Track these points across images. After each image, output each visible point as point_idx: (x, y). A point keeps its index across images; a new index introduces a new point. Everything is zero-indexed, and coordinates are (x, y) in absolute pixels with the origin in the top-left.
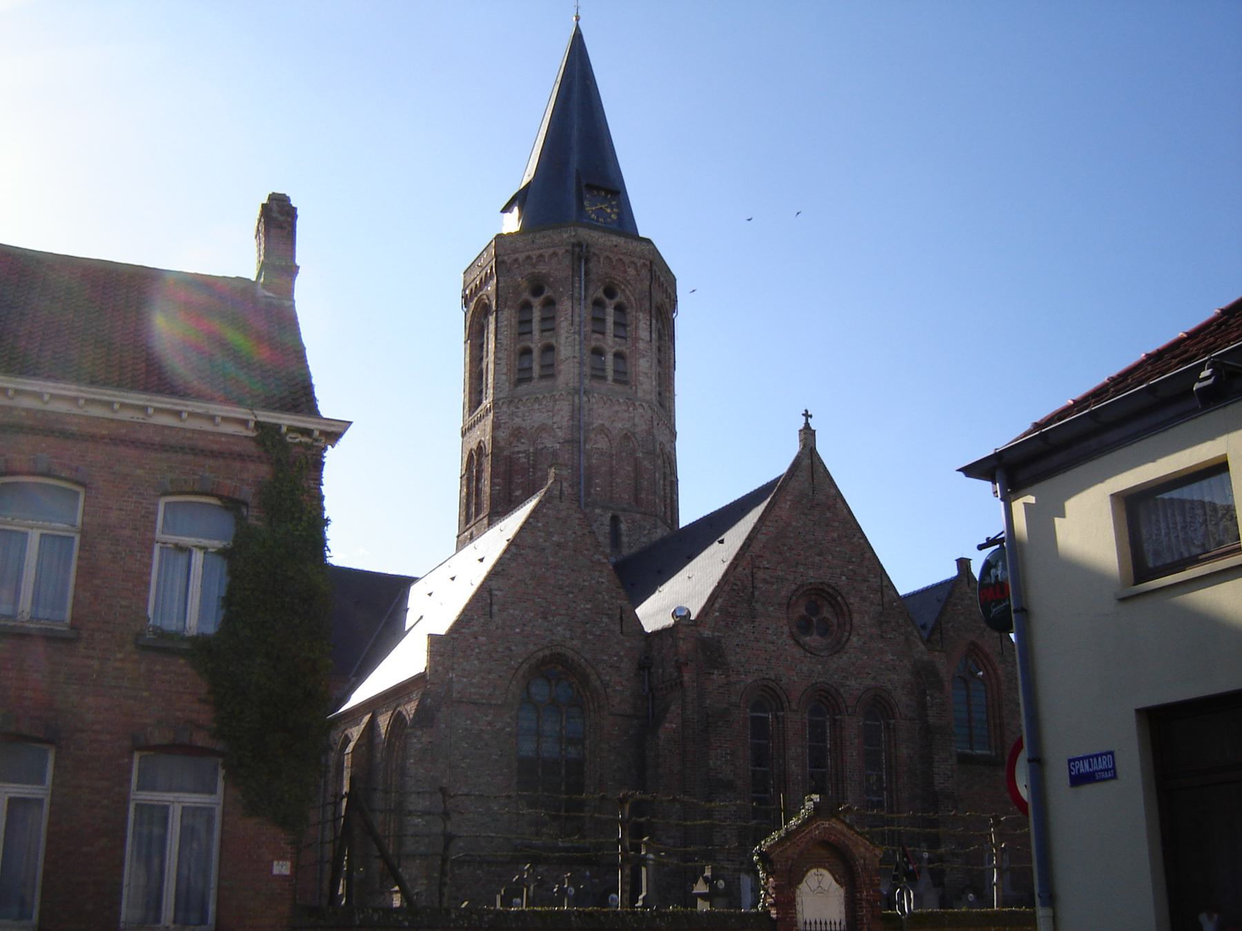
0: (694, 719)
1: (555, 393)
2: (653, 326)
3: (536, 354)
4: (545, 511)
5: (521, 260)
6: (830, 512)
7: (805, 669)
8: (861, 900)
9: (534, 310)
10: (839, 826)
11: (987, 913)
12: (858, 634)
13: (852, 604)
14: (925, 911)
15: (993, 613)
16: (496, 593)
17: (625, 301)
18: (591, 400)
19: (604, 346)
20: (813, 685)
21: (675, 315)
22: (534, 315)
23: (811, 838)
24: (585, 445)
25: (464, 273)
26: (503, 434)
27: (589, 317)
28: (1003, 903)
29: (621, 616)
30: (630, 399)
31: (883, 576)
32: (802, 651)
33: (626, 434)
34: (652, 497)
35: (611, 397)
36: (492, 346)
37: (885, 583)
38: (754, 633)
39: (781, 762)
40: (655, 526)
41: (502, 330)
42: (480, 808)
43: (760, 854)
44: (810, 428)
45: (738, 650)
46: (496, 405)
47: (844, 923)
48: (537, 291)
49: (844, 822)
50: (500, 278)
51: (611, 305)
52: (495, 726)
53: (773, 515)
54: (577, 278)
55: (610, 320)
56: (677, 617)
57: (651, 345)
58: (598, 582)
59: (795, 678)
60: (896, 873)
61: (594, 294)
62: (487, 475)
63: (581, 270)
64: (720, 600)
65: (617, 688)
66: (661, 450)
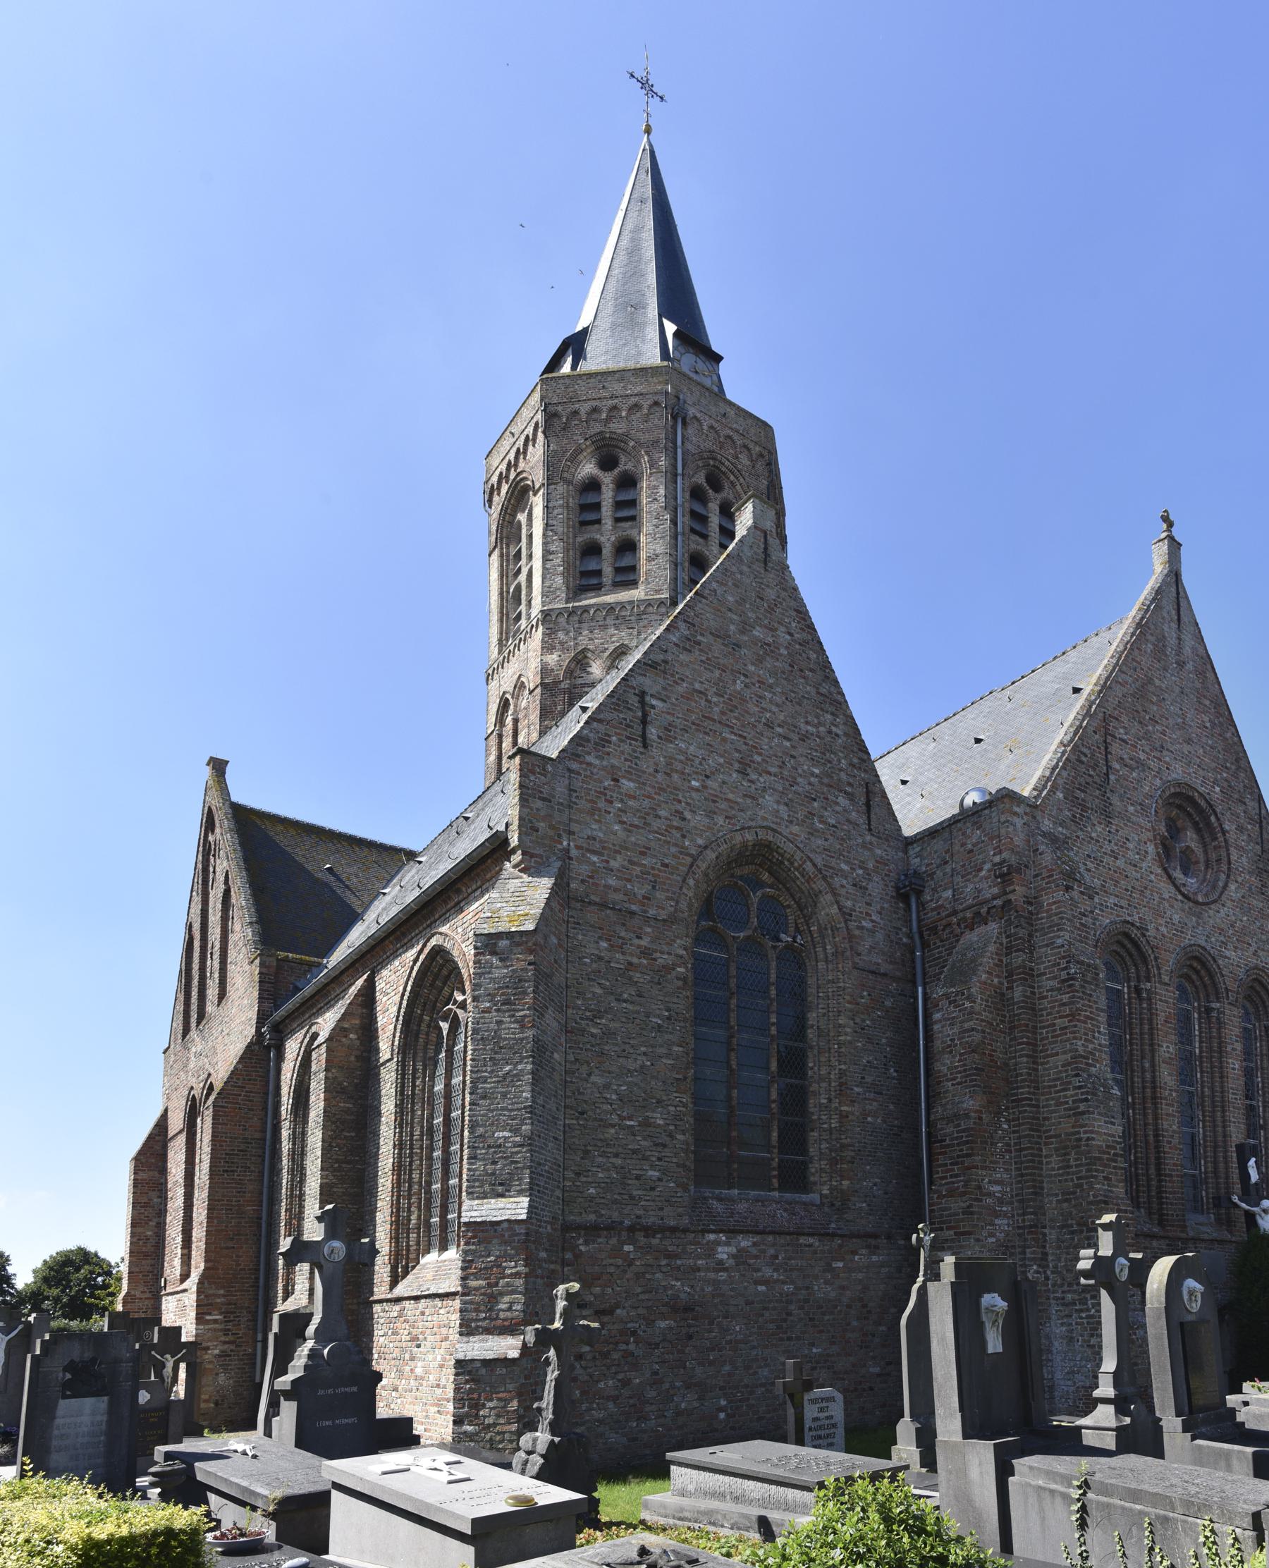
3: (607, 551)
9: (604, 488)
12: (1237, 882)
16: (654, 702)
42: (630, 1119)
46: (548, 618)
52: (655, 960)
58: (830, 732)
65: (864, 923)
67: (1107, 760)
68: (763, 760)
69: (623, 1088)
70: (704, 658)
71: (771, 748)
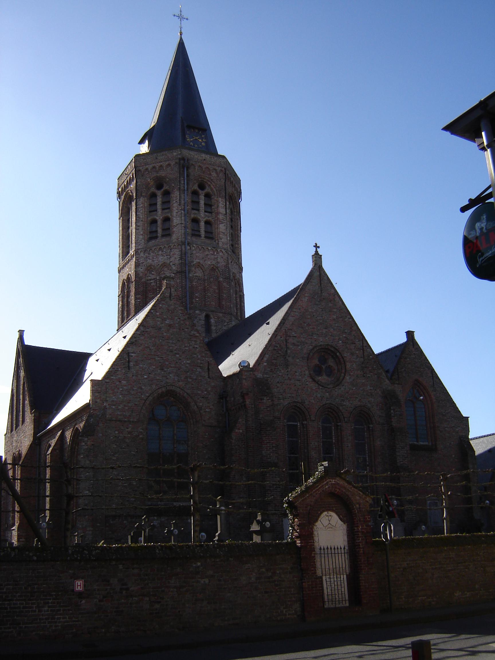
0: (253, 427)
1: (171, 245)
2: (227, 206)
3: (159, 222)
4: (161, 305)
5: (149, 169)
6: (331, 303)
7: (319, 395)
8: (358, 532)
9: (158, 197)
10: (341, 482)
11: (442, 537)
12: (350, 375)
13: (345, 357)
14: (401, 538)
15: (480, 263)
16: (132, 355)
17: (211, 192)
18: (192, 248)
19: (199, 217)
20: (323, 405)
21: (240, 200)
22: (158, 200)
23: (323, 491)
24: (189, 274)
25: (118, 179)
26: (141, 270)
27: (190, 201)
28: (450, 531)
29: (208, 369)
30: (214, 248)
31: (364, 340)
32: (317, 385)
33: (213, 268)
34: (229, 304)
35: (204, 247)
36: (134, 219)
37: (365, 344)
38: (288, 375)
39: (306, 451)
40: (231, 320)
41: (140, 210)
43: (289, 502)
44: (318, 254)
45: (279, 385)
46: (137, 253)
47: (347, 548)
48: (159, 187)
49: (345, 480)
50: (137, 180)
51: (202, 194)
52: (133, 434)
53: (298, 305)
54: (182, 178)
55: (202, 202)
56: (241, 366)
57: (226, 217)
59: (313, 401)
60: (381, 513)
61: (193, 187)
62: (132, 293)
63: (184, 174)
64: (267, 356)
65: (207, 410)
66: (234, 277)
67: (286, 345)
68: (169, 363)
69: (123, 474)
70: (149, 336)
71: (172, 358)
